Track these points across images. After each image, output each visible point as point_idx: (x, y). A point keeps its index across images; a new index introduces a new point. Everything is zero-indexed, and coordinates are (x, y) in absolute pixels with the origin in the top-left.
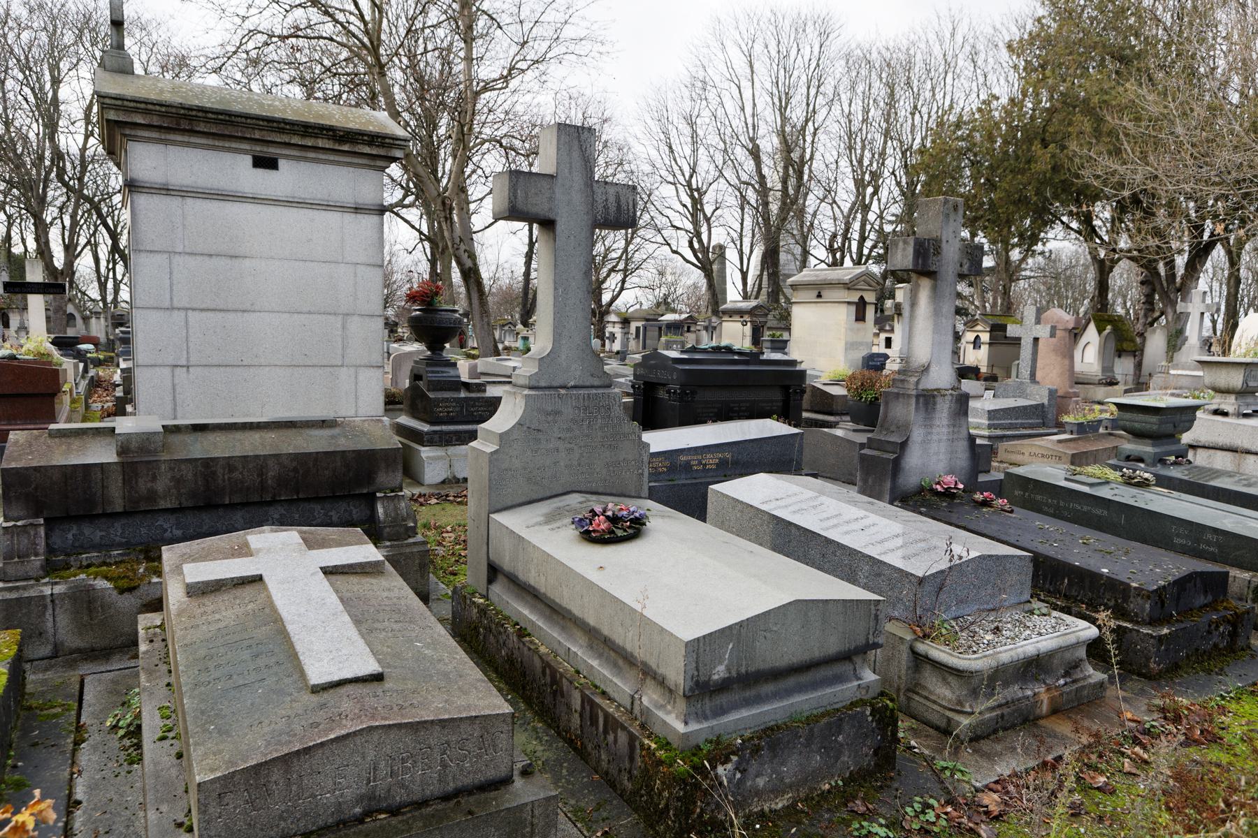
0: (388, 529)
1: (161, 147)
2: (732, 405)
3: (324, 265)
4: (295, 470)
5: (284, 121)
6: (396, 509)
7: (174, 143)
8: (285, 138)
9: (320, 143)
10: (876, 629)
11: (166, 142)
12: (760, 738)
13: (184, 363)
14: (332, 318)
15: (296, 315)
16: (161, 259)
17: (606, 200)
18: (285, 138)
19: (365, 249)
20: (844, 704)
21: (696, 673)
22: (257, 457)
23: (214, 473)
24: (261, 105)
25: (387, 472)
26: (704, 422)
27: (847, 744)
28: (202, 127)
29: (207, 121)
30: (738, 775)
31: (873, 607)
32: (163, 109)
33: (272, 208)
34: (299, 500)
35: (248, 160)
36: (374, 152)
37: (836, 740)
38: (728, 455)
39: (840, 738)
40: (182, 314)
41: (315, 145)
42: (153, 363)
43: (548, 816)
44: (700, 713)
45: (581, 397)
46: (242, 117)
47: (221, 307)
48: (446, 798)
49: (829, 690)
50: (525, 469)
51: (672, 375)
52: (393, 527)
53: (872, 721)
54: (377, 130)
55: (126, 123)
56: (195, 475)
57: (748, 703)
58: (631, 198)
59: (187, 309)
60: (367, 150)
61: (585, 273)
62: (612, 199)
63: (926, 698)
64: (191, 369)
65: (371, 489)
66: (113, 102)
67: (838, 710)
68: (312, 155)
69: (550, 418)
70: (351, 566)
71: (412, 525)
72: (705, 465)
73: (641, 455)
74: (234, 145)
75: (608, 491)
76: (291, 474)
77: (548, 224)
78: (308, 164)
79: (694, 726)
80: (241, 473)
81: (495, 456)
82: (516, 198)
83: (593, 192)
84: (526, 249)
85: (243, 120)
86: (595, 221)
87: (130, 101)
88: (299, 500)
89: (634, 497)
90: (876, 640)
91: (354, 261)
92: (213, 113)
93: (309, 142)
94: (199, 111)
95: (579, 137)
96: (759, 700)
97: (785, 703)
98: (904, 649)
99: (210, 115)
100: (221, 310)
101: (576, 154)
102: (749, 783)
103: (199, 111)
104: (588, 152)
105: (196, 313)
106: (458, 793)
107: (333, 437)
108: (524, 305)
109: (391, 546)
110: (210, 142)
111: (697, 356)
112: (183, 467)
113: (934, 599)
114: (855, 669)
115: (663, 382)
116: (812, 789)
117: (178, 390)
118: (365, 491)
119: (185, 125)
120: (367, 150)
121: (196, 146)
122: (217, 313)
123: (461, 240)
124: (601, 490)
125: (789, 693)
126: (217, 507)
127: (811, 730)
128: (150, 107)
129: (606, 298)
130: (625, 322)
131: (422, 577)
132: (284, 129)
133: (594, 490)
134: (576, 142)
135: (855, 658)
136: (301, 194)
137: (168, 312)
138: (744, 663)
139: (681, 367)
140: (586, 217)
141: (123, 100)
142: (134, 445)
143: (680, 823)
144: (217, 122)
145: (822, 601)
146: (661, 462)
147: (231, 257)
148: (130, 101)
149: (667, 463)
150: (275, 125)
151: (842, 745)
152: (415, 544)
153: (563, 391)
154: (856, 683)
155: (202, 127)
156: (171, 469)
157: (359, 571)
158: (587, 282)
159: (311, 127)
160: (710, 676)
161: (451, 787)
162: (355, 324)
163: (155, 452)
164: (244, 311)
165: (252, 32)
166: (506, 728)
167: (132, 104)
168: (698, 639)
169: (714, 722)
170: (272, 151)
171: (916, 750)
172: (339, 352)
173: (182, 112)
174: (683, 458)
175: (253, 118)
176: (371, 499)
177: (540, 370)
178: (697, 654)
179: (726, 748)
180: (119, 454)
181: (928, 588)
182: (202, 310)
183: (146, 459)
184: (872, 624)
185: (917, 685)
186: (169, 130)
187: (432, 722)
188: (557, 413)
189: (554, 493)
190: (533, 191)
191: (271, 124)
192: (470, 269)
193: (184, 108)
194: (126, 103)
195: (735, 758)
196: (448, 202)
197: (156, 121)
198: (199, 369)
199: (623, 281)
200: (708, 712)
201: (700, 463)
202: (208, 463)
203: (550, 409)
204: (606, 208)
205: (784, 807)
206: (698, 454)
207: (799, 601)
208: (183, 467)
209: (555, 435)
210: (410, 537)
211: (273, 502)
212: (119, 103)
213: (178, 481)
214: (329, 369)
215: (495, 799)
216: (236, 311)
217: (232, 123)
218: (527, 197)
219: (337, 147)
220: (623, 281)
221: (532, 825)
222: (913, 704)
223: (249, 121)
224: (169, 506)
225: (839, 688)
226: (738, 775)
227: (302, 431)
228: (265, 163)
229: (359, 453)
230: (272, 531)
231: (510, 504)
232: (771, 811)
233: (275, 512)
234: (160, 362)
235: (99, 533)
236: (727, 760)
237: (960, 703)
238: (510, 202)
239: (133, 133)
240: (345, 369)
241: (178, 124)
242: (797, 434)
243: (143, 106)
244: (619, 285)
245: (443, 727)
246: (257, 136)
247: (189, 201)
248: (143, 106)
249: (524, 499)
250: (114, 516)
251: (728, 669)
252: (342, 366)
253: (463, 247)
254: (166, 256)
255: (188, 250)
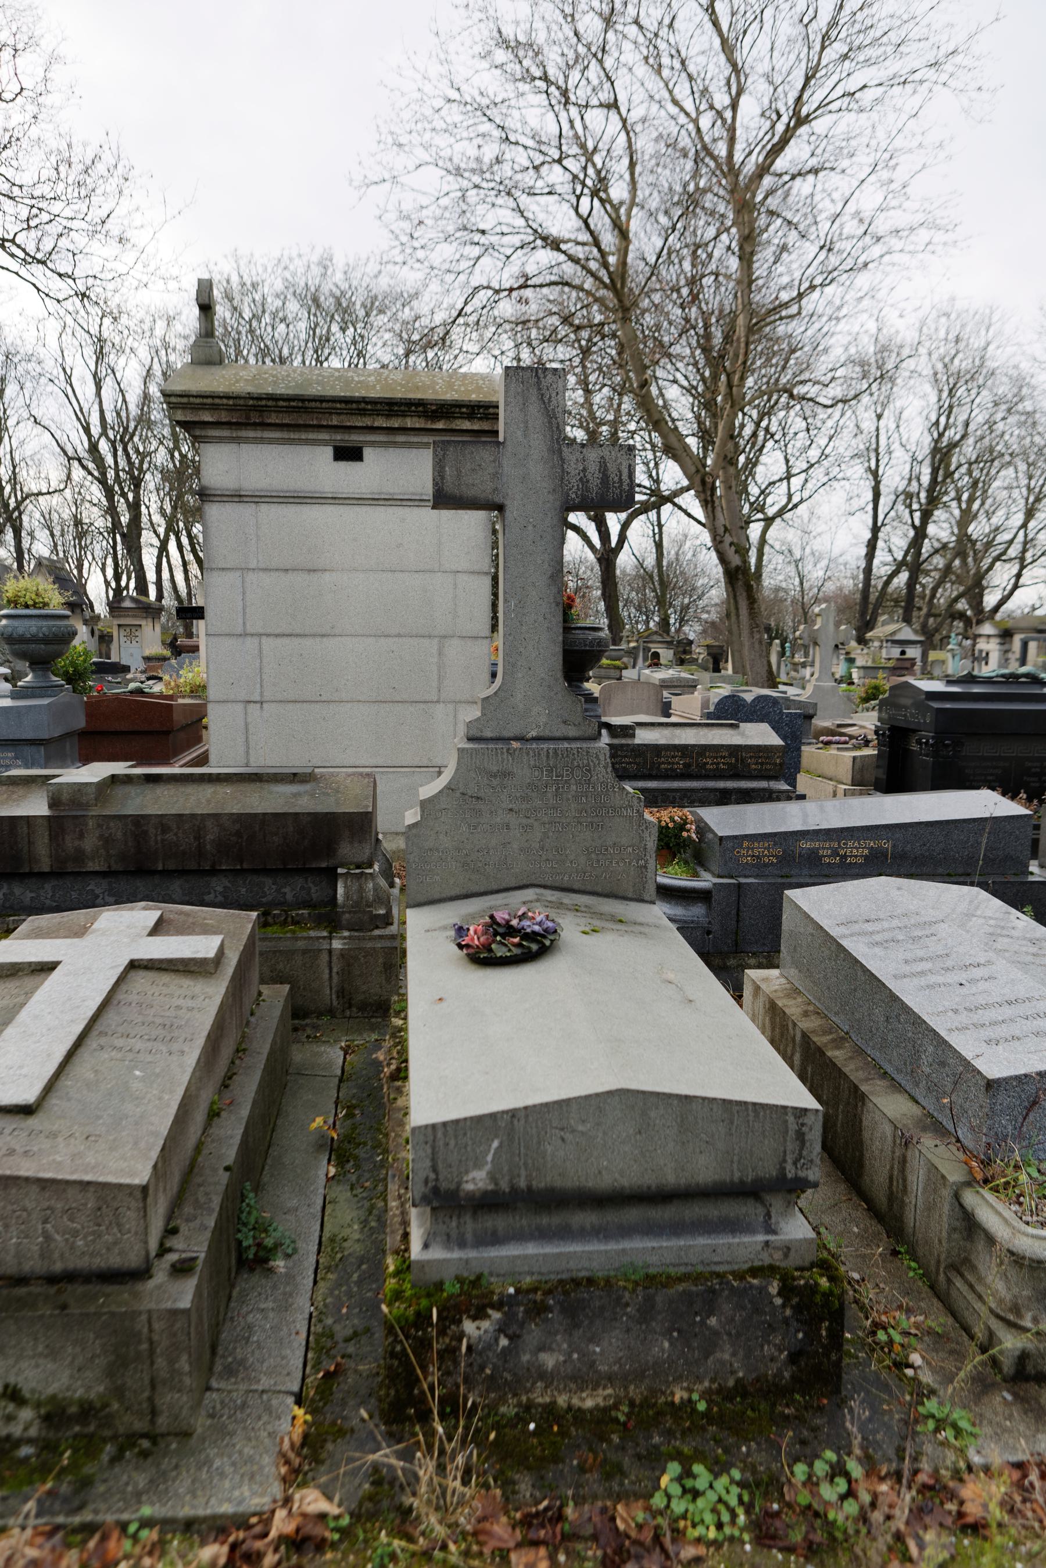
0: (347, 916)
1: (233, 447)
2: (1028, 764)
3: (417, 575)
4: (238, 834)
5: (364, 400)
6: (361, 889)
7: (247, 440)
8: (367, 421)
9: (409, 423)
10: (800, 1156)
11: (238, 440)
12: (549, 1292)
13: (258, 698)
14: (426, 642)
15: (382, 639)
16: (234, 577)
17: (584, 470)
18: (367, 421)
19: (468, 553)
20: (736, 1267)
21: (432, 1176)
22: (193, 816)
23: (146, 832)
24: (348, 382)
25: (351, 843)
26: (978, 788)
27: (729, 1334)
28: (273, 419)
29: (278, 410)
30: (504, 1342)
31: (791, 1119)
32: (231, 402)
33: (357, 509)
34: (243, 871)
35: (329, 451)
36: (476, 427)
37: (703, 1323)
38: (886, 845)
39: (713, 1321)
40: (256, 640)
41: (403, 425)
42: (225, 698)
43: (175, 1335)
44: (454, 1234)
45: (543, 754)
46: (315, 401)
47: (298, 631)
48: (52, 1279)
49: (702, 1241)
50: (459, 850)
51: (924, 717)
52: (355, 912)
53: (784, 1306)
54: (481, 397)
55: (195, 423)
56: (125, 834)
57: (543, 1235)
58: (625, 464)
59: (260, 635)
60: (466, 425)
61: (552, 577)
62: (593, 468)
63: (971, 1287)
64: (265, 705)
65: (331, 863)
66: (179, 400)
67: (718, 1275)
68: (401, 438)
69: (495, 782)
70: (170, 961)
71: (382, 912)
72: (845, 856)
73: (642, 839)
74: (312, 436)
75: (589, 888)
76: (234, 839)
77: (500, 508)
78: (398, 450)
79: (437, 1253)
80: (176, 834)
81: (414, 831)
82: (442, 478)
83: (563, 460)
84: (868, 535)
85: (318, 404)
86: (567, 502)
87: (196, 397)
88: (243, 871)
89: (625, 898)
90: (802, 1174)
91: (454, 568)
92: (284, 400)
93: (396, 423)
94: (268, 399)
95: (539, 383)
96: (565, 1233)
97: (612, 1246)
98: (946, 1193)
99: (281, 403)
100: (297, 635)
101: (534, 409)
102: (525, 1358)
103: (268, 399)
104: (554, 402)
105: (271, 640)
106: (70, 1277)
107: (296, 795)
108: (863, 613)
109: (350, 938)
110: (285, 435)
111: (977, 689)
112: (112, 824)
113: (1020, 1119)
114: (768, 1215)
115: (912, 727)
116: (653, 1392)
117: (251, 730)
118: (324, 865)
119: (255, 418)
120: (466, 425)
121: (271, 441)
122: (294, 639)
123: (726, 530)
124: (576, 887)
125: (626, 1231)
126: (153, 873)
127: (649, 1300)
128: (217, 401)
129: (990, 600)
130: (1006, 635)
131: (388, 980)
132: (365, 410)
133: (565, 885)
134: (534, 391)
135: (768, 1198)
136: (391, 489)
137: (241, 639)
138: (523, 1173)
139: (936, 705)
140: (551, 497)
141: (188, 396)
142: (65, 797)
143: (397, 1391)
144: (290, 410)
145: (679, 1097)
146: (768, 848)
147: (309, 571)
148: (196, 397)
149: (779, 852)
150: (354, 406)
151: (716, 1333)
152: (381, 937)
153: (515, 745)
154: (761, 1238)
155: (273, 419)
156: (99, 826)
157: (181, 968)
158: (554, 590)
159: (396, 404)
160: (459, 1184)
161: (58, 1267)
162: (453, 648)
163: (86, 806)
164: (323, 636)
165: (476, 289)
166: (134, 1204)
167: (198, 401)
168: (434, 1126)
169: (471, 1254)
170: (355, 438)
171: (909, 1372)
172: (435, 684)
173: (251, 402)
174: (806, 845)
175: (328, 401)
176: (331, 876)
177: (484, 714)
178: (433, 1148)
179: (483, 1296)
180: (50, 807)
181: (1003, 1099)
182: (277, 636)
183: (74, 813)
184: (791, 1146)
185: (967, 1261)
186: (238, 425)
187: (27, 1179)
188: (506, 774)
189: (504, 885)
190: (468, 466)
191: (349, 406)
192: (738, 568)
193: (252, 398)
194: (192, 400)
195: (496, 1315)
196: (709, 480)
197: (224, 417)
198: (273, 705)
199: (1019, 576)
200: (469, 1236)
201: (835, 853)
202: (139, 821)
203: (495, 769)
204: (584, 481)
205: (597, 1407)
206: (831, 840)
207: (628, 1091)
208: (112, 824)
209: (504, 805)
210: (377, 927)
211: (214, 872)
212: (185, 400)
213: (107, 841)
214: (422, 706)
215: (107, 1296)
216: (314, 635)
217: (306, 410)
218: (459, 476)
219: (429, 426)
220: (1019, 576)
221: (151, 1342)
222: (954, 1293)
223: (324, 405)
224: (97, 868)
225: (723, 1240)
226: (504, 1342)
227: (266, 786)
228: (348, 454)
229: (315, 816)
230: (145, 909)
231: (437, 896)
232: (570, 1408)
233: (218, 885)
234: (232, 697)
235: (29, 895)
236: (479, 1315)
237: (1016, 1309)
238: (435, 484)
239: (203, 433)
240: (442, 705)
241: (248, 418)
242: (1026, 816)
243: (209, 401)
244: (1013, 581)
245: (43, 1189)
246: (335, 423)
247: (264, 507)
248: (209, 401)
249: (457, 891)
250: (42, 875)
251: (492, 1177)
252: (438, 702)
253: (728, 539)
254: (238, 573)
255: (262, 565)
